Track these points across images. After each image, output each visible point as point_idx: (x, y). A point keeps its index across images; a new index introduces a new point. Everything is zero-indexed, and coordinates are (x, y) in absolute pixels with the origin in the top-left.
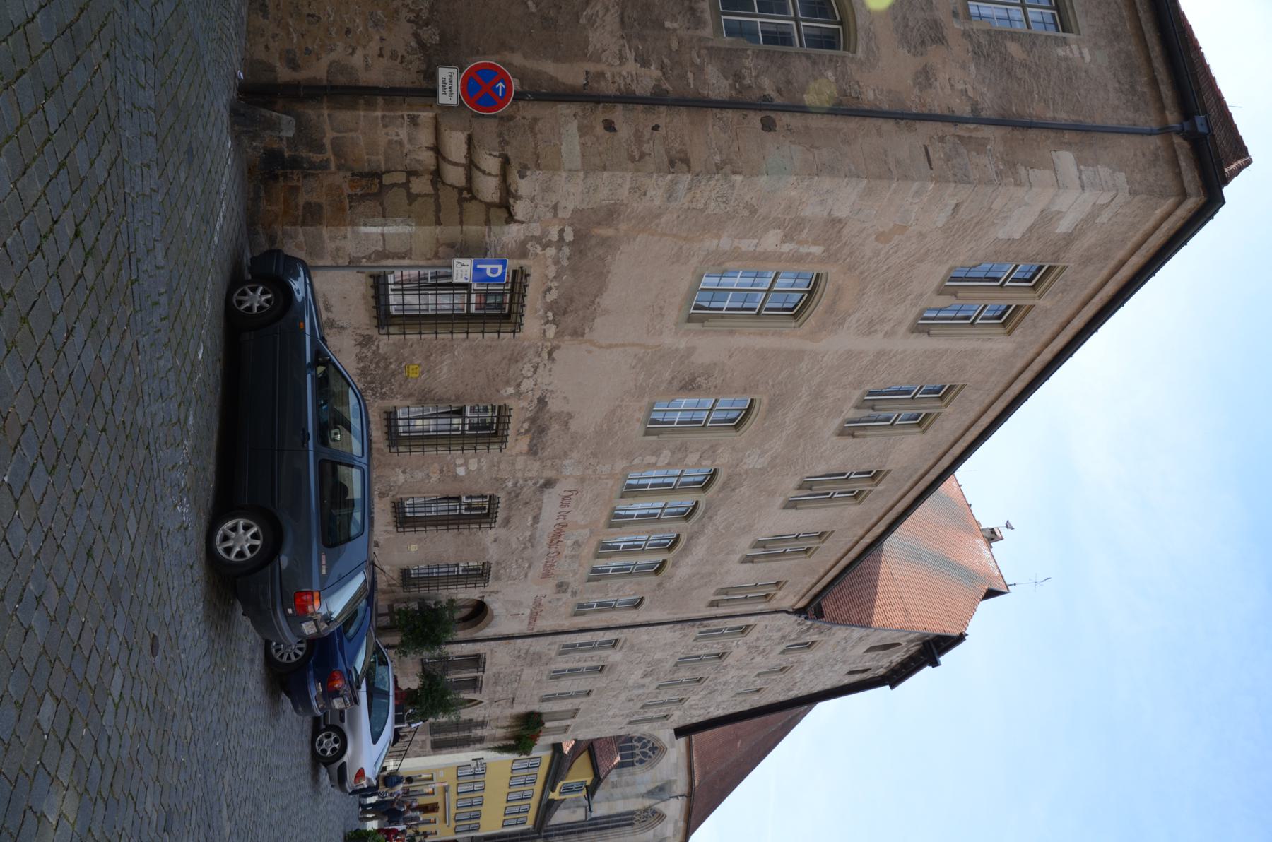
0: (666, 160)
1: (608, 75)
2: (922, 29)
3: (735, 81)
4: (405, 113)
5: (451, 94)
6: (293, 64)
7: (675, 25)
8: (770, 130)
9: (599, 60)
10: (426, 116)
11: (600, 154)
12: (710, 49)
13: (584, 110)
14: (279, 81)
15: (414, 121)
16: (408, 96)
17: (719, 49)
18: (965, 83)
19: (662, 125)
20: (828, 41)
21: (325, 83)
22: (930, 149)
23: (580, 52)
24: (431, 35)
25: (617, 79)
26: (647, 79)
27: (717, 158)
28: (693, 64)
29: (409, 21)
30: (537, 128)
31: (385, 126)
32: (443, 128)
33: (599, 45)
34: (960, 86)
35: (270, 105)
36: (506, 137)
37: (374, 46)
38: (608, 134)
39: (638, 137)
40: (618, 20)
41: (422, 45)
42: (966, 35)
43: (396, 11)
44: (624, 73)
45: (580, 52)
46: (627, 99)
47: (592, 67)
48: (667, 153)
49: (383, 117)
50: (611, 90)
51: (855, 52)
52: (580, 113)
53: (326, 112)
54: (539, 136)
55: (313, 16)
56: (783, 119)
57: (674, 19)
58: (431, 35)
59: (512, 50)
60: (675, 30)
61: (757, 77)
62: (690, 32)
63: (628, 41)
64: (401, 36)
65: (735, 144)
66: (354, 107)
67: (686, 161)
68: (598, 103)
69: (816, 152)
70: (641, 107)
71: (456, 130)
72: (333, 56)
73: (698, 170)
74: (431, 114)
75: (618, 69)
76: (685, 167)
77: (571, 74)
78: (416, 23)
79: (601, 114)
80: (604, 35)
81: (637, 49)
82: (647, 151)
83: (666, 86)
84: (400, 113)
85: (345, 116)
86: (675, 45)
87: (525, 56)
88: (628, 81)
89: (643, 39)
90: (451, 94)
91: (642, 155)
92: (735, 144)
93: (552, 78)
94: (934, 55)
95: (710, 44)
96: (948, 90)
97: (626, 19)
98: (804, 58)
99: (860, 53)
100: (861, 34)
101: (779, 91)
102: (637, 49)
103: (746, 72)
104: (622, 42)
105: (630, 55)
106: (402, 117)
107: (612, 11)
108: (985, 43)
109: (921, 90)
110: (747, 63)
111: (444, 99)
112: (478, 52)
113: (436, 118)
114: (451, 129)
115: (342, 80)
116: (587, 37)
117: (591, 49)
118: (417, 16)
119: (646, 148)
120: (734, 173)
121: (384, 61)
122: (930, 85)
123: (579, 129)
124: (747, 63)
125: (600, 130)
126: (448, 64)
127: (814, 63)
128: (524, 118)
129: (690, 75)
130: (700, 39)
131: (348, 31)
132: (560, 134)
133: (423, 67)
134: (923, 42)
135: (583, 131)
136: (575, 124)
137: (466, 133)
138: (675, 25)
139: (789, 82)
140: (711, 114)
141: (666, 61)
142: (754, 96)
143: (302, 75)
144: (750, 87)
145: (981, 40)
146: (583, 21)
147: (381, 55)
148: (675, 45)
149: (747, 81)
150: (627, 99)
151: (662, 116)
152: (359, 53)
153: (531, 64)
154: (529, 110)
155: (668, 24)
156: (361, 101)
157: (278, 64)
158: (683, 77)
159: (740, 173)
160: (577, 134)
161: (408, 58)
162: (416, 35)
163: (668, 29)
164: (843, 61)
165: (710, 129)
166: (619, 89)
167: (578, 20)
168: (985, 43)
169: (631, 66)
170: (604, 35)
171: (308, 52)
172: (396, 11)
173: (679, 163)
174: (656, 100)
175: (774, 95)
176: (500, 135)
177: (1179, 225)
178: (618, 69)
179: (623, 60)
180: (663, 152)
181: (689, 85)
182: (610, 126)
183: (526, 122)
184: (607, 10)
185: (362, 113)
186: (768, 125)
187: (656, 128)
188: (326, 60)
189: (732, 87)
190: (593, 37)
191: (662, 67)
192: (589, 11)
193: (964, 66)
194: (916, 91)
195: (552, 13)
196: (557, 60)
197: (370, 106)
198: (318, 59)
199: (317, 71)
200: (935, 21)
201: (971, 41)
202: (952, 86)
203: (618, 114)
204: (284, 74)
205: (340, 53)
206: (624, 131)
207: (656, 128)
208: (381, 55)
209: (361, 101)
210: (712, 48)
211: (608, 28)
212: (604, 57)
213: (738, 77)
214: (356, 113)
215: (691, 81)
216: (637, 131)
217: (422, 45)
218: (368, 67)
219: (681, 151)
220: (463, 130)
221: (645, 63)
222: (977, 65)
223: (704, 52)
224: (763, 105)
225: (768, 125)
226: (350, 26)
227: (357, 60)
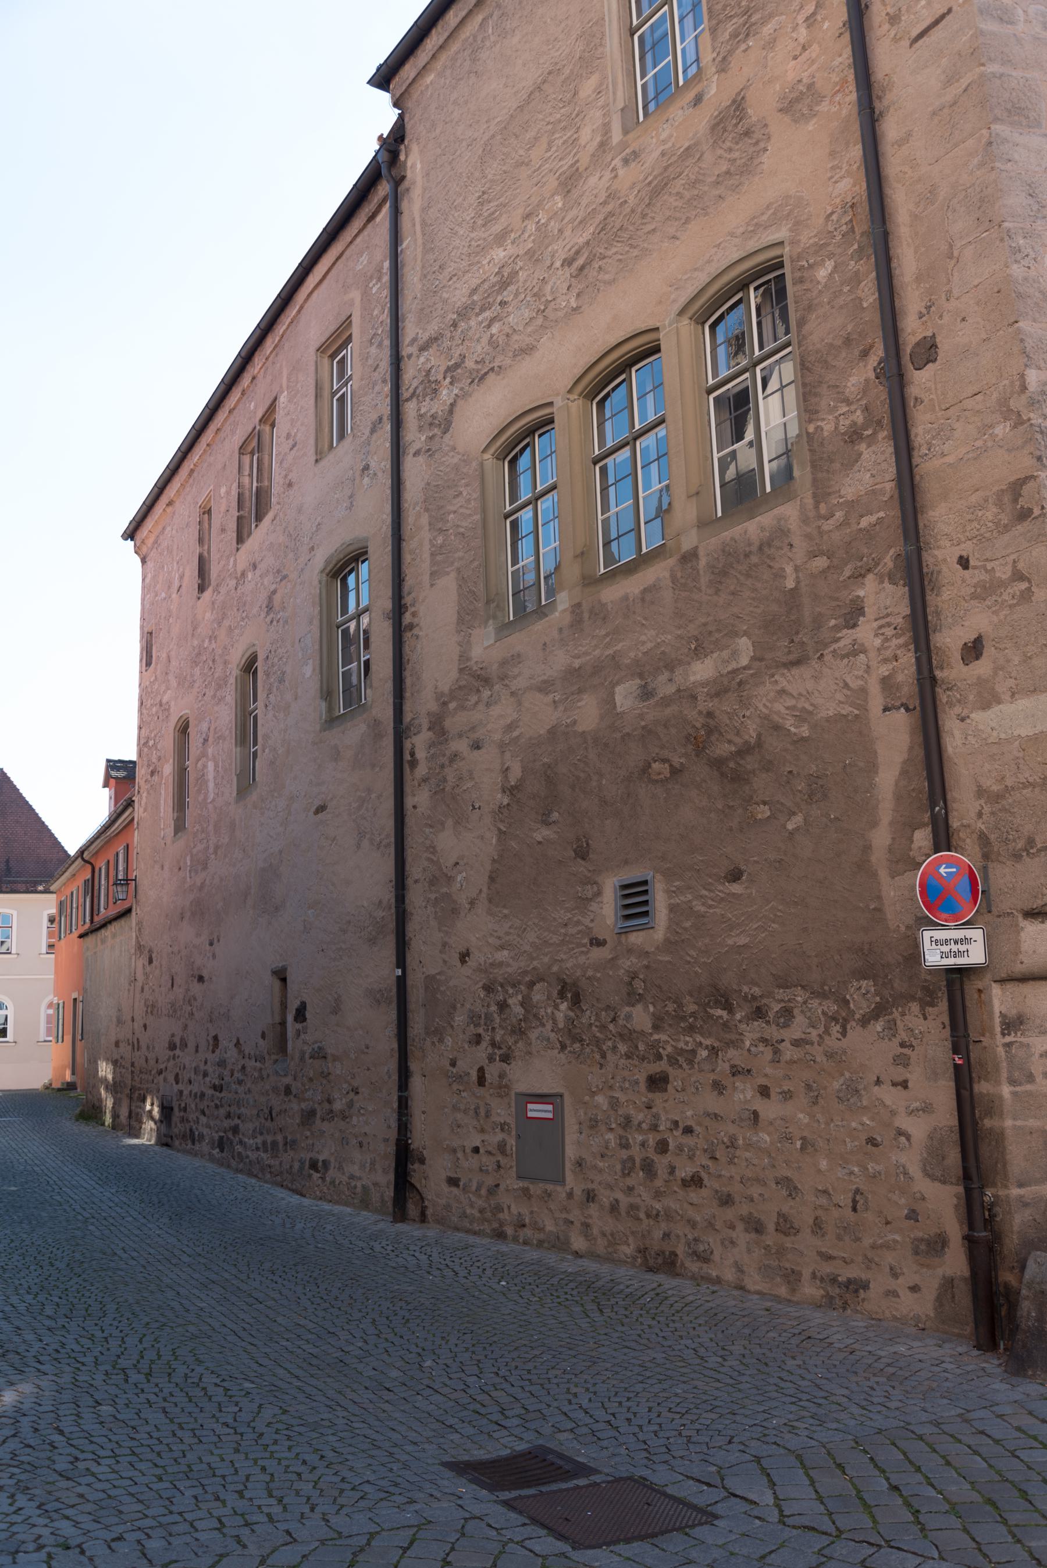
0: (1020, 528)
1: (884, 670)
2: (728, 144)
3: (861, 437)
4: (1000, 1040)
5: (966, 940)
6: (937, 1244)
7: (789, 570)
8: (934, 346)
9: (863, 690)
10: (1000, 1000)
11: (1027, 659)
12: (818, 500)
13: (951, 705)
14: (967, 1273)
15: (1013, 1024)
16: (967, 1036)
17: (815, 481)
18: (795, 28)
19: (957, 552)
20: (776, 293)
21: (961, 1189)
22: (915, 33)
23: (852, 728)
24: (861, 995)
25: (888, 653)
26: (883, 598)
27: (1002, 430)
28: (845, 523)
29: (844, 1033)
30: (995, 788)
31: (1031, 1078)
32: (1018, 969)
33: (839, 696)
34: (803, 33)
35: (1012, 1297)
36: (1020, 844)
37: (889, 1095)
38: (989, 651)
39: (984, 592)
40: (795, 671)
41: (878, 1011)
42: (723, 65)
43: (830, 1055)
44: (878, 642)
45: (852, 728)
46: (921, 627)
47: (876, 701)
48: (1007, 528)
49: (1012, 1082)
50: (908, 659)
51: (781, 243)
52: (957, 709)
53: (1015, 1192)
54: (1009, 782)
55: (855, 1202)
56: (913, 329)
57: (780, 575)
58: (861, 995)
59: (867, 848)
60: (797, 569)
61: (848, 402)
62: (796, 541)
63: (826, 645)
64: (868, 1047)
65: (969, 404)
66: (999, 1138)
67: (1016, 488)
68: (933, 680)
69: (958, 244)
70: (930, 598)
71: (1018, 943)
72: (915, 1171)
73: (1029, 462)
74: (996, 990)
75: (872, 654)
76: (1026, 490)
77: (893, 737)
78: (846, 1021)
79: (954, 672)
80: (818, 690)
81: (837, 628)
82: (1009, 570)
83: (888, 563)
84: (1001, 1051)
85: (1017, 1156)
86: (821, 562)
87: (874, 824)
88: (889, 632)
89: (818, 622)
90: (966, 940)
91: (1019, 576)
92: (969, 404)
93: (904, 773)
94: (762, 105)
95: (809, 501)
96: (814, 50)
97: (791, 657)
98: (807, 328)
99: (782, 233)
100: (752, 245)
101: (865, 354)
102: (837, 628)
103: (845, 423)
104: (828, 658)
105: (847, 637)
106: (1008, 1045)
107: (783, 683)
108: (730, 27)
109: (820, 98)
110: (828, 427)
111: (976, 955)
112: (878, 910)
113: (1002, 981)
114: (1017, 952)
115: (954, 1156)
116: (828, 720)
117: (846, 710)
118: (834, 1019)
119: (1004, 573)
120: (1024, 388)
121: (915, 1075)
122: (810, 86)
123: (986, 706)
124: (828, 427)
125: (982, 668)
126: (915, 955)
127: (810, 308)
128: (980, 815)
129: (864, 522)
130: (805, 520)
131: (872, 1142)
132: (999, 743)
133: (915, 1007)
134: (747, 133)
135: (988, 699)
136: (978, 716)
137: (1023, 923)
138: (789, 570)
139: (848, 341)
140: (927, 466)
141: (847, 572)
142: (880, 394)
143: (954, 1230)
144: (866, 409)
145: (727, 35)
146: (805, 731)
147: (904, 1085)
148: (821, 562)
149: (859, 417)
150: (921, 627)
151: (942, 555)
152: (904, 1122)
153: (886, 812)
154: (965, 808)
155: (790, 584)
156: (987, 1123)
157: (940, 1272)
158: (868, 534)
159: (1022, 376)
160: (996, 709)
161: (903, 1035)
162: (864, 1022)
163: (798, 582)
164: (799, 257)
165: (950, 459)
166: (906, 645)
167: (803, 739)
168: (730, 27)
169: (865, 632)
170: (818, 690)
171: (913, 1215)
172: (830, 1055)
173: (1022, 502)
174: (916, 578)
175: (873, 360)
176: (1017, 857)
177: (282, 317)
178: (872, 654)
179: (857, 650)
180: (1006, 537)
181: (880, 521)
182: (974, 650)
183: (987, 809)
184: (783, 692)
185: (1009, 1123)
186: (928, 351)
187: (964, 562)
188: (923, 1185)
189: (871, 440)
190: (830, 710)
191: (859, 576)
192: (789, 724)
193: (771, 44)
194: (824, 107)
195: (801, 786)
196: (872, 768)
197: (993, 1106)
198: (924, 1199)
199: (943, 1202)
200: (713, 128)
201: (730, 52)
202: (804, 48)
203: (950, 639)
204: (955, 1262)
205: (911, 1160)
206: (978, 621)
207: (964, 562)
208: (904, 1085)
209: (987, 1123)
210: (815, 495)
211: (810, 685)
212: (854, 684)
213: (854, 436)
214: (1009, 1132)
215: (873, 519)
216: (974, 596)
217: (878, 1011)
218: (927, 1109)
219: (999, 503)
220: (1018, 930)
221: (854, 613)
222: (764, 21)
223: (823, 509)
224: (894, 375)
225: (928, 351)
226: (864, 1137)
227: (918, 1128)
